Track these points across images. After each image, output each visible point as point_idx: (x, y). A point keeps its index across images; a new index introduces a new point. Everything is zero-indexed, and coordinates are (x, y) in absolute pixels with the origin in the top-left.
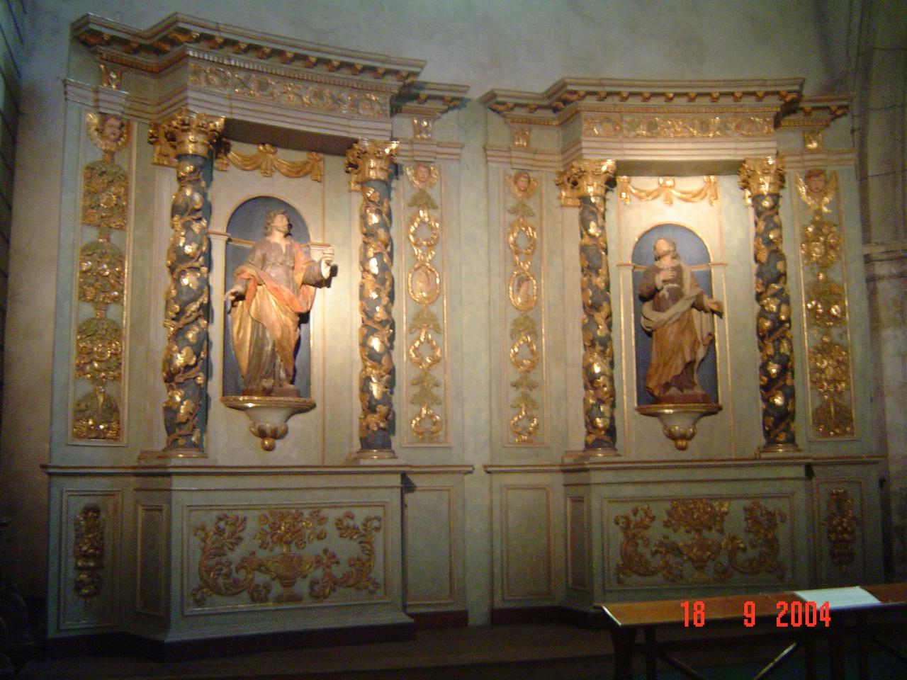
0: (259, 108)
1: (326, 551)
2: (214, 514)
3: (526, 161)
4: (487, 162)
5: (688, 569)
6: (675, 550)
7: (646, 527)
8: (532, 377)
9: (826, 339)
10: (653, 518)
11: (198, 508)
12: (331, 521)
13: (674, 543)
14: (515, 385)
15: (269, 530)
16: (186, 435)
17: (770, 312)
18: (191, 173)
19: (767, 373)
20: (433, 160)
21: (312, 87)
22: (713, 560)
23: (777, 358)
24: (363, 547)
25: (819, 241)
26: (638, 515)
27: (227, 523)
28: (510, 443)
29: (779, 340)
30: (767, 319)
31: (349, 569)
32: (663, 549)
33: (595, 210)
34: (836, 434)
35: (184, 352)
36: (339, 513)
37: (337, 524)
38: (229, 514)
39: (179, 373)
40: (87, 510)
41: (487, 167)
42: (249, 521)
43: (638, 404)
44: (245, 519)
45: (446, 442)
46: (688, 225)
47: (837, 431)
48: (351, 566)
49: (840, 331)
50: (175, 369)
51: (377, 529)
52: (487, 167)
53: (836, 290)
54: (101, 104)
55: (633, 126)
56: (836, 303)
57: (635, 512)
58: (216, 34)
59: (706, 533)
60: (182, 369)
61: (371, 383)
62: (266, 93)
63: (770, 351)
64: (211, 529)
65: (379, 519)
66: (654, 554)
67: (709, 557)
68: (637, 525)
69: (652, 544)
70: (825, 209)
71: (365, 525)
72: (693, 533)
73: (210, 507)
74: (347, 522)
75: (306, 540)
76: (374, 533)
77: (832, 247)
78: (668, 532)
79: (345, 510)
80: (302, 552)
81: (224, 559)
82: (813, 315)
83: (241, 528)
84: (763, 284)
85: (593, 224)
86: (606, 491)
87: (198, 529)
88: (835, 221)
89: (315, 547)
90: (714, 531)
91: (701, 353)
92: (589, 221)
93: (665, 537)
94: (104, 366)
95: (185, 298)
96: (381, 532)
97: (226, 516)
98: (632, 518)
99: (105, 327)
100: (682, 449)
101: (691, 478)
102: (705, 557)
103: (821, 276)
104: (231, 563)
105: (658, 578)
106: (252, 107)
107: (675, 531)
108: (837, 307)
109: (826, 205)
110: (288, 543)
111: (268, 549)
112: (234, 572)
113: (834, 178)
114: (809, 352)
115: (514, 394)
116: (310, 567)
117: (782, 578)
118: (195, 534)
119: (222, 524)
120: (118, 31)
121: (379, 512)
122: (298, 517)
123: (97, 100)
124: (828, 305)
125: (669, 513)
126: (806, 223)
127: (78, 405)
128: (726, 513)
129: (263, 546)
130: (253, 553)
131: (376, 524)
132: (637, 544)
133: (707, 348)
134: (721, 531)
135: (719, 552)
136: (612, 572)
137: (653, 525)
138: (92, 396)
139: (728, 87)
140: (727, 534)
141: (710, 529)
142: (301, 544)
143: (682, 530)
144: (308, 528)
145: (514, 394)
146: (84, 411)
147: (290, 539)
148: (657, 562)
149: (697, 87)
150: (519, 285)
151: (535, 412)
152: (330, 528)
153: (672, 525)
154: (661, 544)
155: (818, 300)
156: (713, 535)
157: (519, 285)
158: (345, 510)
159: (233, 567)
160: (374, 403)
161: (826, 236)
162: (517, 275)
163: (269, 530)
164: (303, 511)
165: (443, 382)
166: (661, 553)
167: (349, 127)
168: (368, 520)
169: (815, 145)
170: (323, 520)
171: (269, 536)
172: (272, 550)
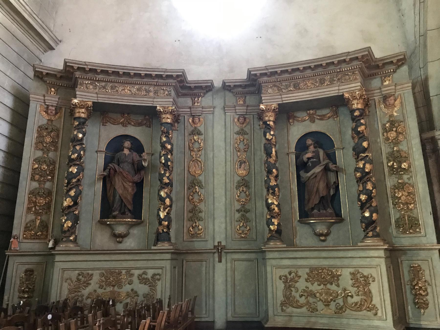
0: (111, 97)
1: (132, 290)
2: (77, 272)
3: (242, 111)
4: (225, 113)
5: (320, 306)
6: (313, 295)
7: (297, 282)
8: (247, 207)
9: (400, 181)
10: (300, 277)
11: (68, 269)
12: (136, 275)
13: (311, 291)
14: (238, 211)
15: (104, 280)
16: (67, 237)
17: (359, 168)
18: (78, 125)
19: (360, 200)
20: (200, 114)
21: (137, 87)
22: (335, 301)
23: (364, 191)
24: (150, 288)
25: (393, 130)
26: (292, 275)
27: (83, 277)
28: (235, 238)
29: (366, 182)
30: (358, 172)
31: (143, 299)
32: (306, 294)
33: (269, 127)
34: (411, 233)
35: (67, 199)
36: (140, 272)
37: (138, 277)
38: (85, 272)
39: (66, 209)
40: (26, 271)
41: (225, 115)
42: (94, 275)
43: (300, 218)
44: (92, 275)
45: (205, 238)
46: (323, 131)
47: (411, 231)
48: (144, 297)
49: (409, 176)
50: (64, 208)
51: (159, 280)
52: (225, 115)
53: (404, 155)
54: (46, 101)
55: (287, 87)
56: (405, 162)
57: (290, 273)
58: (86, 67)
59: (329, 286)
60: (67, 208)
61: (160, 212)
62: (114, 91)
63: (361, 188)
64: (74, 279)
65: (159, 274)
66: (301, 296)
67: (331, 300)
68: (291, 280)
69: (300, 291)
70: (395, 114)
71: (152, 277)
72: (322, 286)
73: (75, 269)
74: (144, 276)
75: (123, 284)
76: (157, 281)
77: (400, 133)
78: (309, 284)
79: (143, 270)
80: (121, 290)
81: (80, 294)
82: (392, 169)
83: (90, 279)
84: (355, 154)
85: (268, 134)
86: (274, 262)
87: (67, 279)
88: (402, 120)
89: (127, 288)
90: (333, 285)
91: (332, 192)
92: (267, 133)
93: (307, 287)
94: (41, 208)
95: (70, 177)
96: (161, 281)
97: (83, 273)
98: (289, 277)
99: (43, 191)
100: (324, 241)
101: (295, 260)
102: (329, 300)
103: (395, 149)
104: (83, 296)
105: (304, 309)
106: (107, 96)
107: (312, 284)
108: (405, 164)
109: (395, 112)
110: (114, 286)
111: (103, 289)
112: (85, 300)
113: (400, 97)
114: (391, 188)
115: (237, 215)
116: (124, 298)
117: (376, 314)
118: (66, 282)
119: (81, 277)
120: (50, 71)
121: (160, 271)
122: (120, 273)
123: (44, 100)
124: (400, 163)
125: (307, 274)
126: (385, 122)
127: (27, 224)
128: (340, 275)
129: (101, 287)
130: (95, 291)
131: (158, 277)
132: (292, 291)
133: (335, 189)
134: (338, 286)
135: (337, 297)
136: (279, 305)
137: (300, 280)
138: (34, 221)
139: (330, 60)
140: (341, 287)
141: (331, 284)
142: (120, 287)
143: (316, 283)
144: (123, 279)
145: (237, 215)
146: (28, 227)
147: (114, 284)
148: (302, 300)
149: (314, 62)
150: (240, 165)
151: (248, 223)
152: (135, 279)
153: (310, 281)
154: (304, 291)
155: (394, 161)
156: (333, 287)
157: (240, 165)
158: (143, 270)
159: (84, 297)
160: (161, 220)
161: (397, 128)
162: (239, 161)
163: (104, 280)
164: (122, 271)
165: (204, 210)
166: (304, 295)
167: (153, 102)
168: (155, 275)
169: (387, 83)
170: (132, 275)
171: (104, 283)
172: (105, 289)
